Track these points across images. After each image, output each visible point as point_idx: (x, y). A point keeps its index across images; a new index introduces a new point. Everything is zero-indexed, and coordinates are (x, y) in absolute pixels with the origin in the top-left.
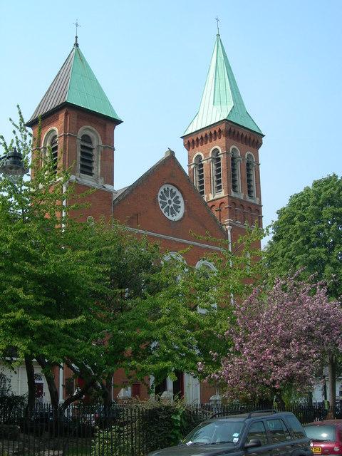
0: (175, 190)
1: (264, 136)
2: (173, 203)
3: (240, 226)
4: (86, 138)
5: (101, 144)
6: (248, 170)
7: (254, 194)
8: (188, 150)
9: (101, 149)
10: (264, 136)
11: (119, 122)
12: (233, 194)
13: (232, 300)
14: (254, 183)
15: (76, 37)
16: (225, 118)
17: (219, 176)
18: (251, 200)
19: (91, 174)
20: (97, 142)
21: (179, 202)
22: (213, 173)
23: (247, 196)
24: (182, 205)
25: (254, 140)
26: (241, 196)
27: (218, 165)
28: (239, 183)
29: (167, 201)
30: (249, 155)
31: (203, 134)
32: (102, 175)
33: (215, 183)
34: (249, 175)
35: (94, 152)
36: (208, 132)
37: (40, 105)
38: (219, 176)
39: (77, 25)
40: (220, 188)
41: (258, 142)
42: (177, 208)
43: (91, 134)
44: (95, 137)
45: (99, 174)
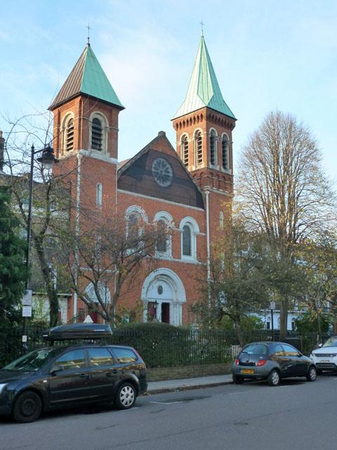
3: (223, 193)
5: (108, 126)
7: (228, 167)
9: (108, 129)
14: (228, 158)
20: (105, 124)
35: (103, 132)
40: (201, 161)
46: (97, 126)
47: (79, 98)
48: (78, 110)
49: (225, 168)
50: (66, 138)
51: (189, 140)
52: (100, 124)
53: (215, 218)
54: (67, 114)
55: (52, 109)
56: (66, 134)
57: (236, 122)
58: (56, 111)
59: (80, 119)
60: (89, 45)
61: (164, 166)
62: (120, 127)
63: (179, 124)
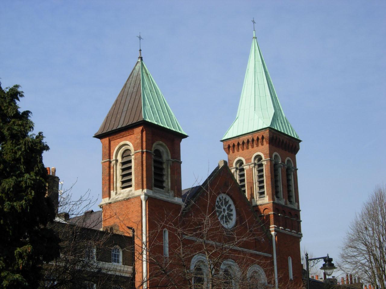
1: (300, 141)
2: (226, 212)
3: (289, 233)
4: (158, 153)
5: (170, 158)
6: (288, 175)
7: (293, 199)
9: (170, 163)
10: (300, 141)
11: (185, 136)
12: (276, 201)
14: (293, 189)
15: (140, 50)
16: (269, 126)
17: (261, 182)
18: (289, 205)
19: (162, 187)
20: (166, 156)
21: (231, 210)
22: (256, 179)
23: (288, 202)
24: (234, 212)
25: (292, 146)
26: (282, 202)
27: (261, 171)
28: (281, 188)
29: (222, 210)
30: (288, 161)
32: (172, 188)
33: (258, 188)
34: (288, 180)
35: (164, 166)
36: (250, 137)
38: (261, 182)
39: (140, 38)
40: (263, 193)
41: (296, 147)
42: (230, 215)
43: (161, 149)
44: (164, 151)
45: (170, 187)
46: (158, 159)
47: (141, 128)
48: (139, 141)
49: (291, 202)
50: (119, 172)
51: (246, 167)
52: (161, 157)
53: (283, 267)
54: (122, 143)
55: (100, 136)
56: (119, 167)
57: (300, 144)
58: (106, 140)
59: (142, 153)
60: (141, 58)
61: (226, 203)
62: (182, 159)
63: (231, 145)
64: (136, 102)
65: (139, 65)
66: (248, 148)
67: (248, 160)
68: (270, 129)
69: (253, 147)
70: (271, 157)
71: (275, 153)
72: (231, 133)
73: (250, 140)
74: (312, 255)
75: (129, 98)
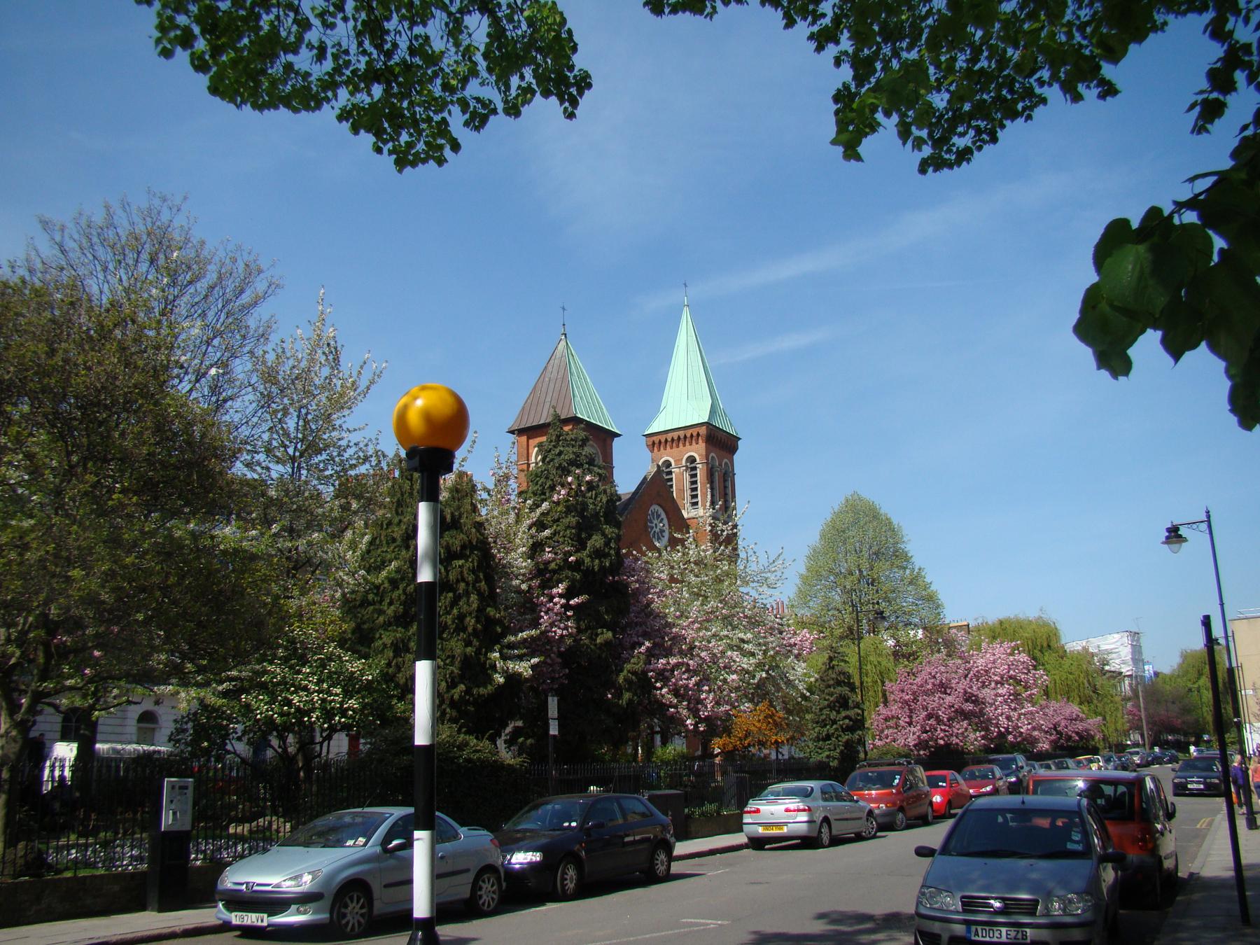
0: (663, 515)
6: (725, 481)
8: (652, 451)
11: (618, 435)
13: (461, 562)
22: (687, 485)
30: (726, 464)
31: (675, 435)
36: (682, 433)
37: (523, 408)
39: (564, 309)
40: (696, 503)
58: (524, 438)
61: (659, 516)
64: (564, 391)
65: (563, 343)
66: (678, 446)
67: (678, 461)
68: (707, 424)
69: (684, 445)
70: (707, 459)
71: (712, 454)
72: (656, 427)
73: (682, 437)
74: (260, 286)
75: (552, 385)
